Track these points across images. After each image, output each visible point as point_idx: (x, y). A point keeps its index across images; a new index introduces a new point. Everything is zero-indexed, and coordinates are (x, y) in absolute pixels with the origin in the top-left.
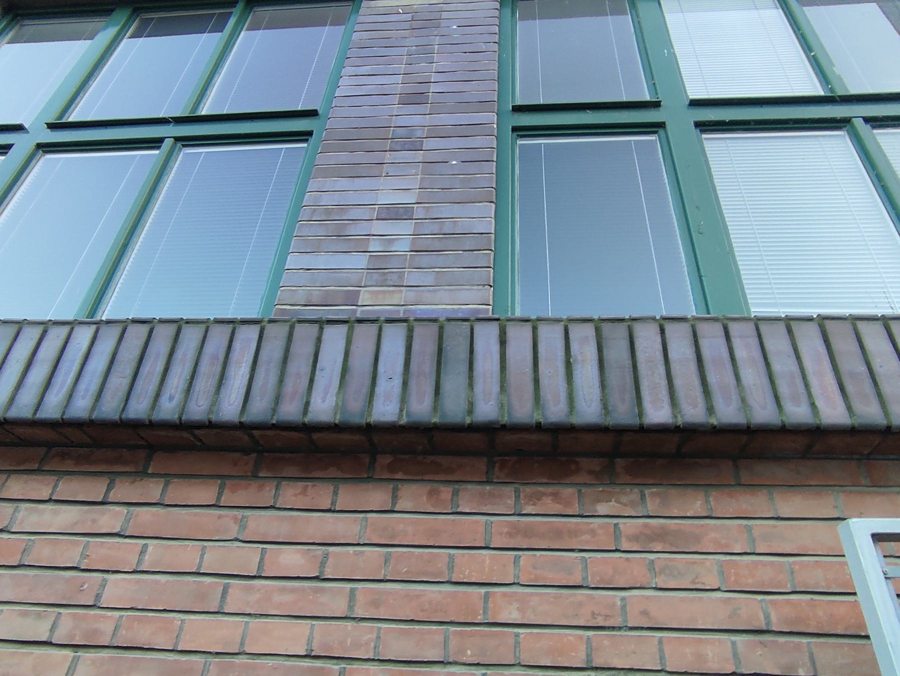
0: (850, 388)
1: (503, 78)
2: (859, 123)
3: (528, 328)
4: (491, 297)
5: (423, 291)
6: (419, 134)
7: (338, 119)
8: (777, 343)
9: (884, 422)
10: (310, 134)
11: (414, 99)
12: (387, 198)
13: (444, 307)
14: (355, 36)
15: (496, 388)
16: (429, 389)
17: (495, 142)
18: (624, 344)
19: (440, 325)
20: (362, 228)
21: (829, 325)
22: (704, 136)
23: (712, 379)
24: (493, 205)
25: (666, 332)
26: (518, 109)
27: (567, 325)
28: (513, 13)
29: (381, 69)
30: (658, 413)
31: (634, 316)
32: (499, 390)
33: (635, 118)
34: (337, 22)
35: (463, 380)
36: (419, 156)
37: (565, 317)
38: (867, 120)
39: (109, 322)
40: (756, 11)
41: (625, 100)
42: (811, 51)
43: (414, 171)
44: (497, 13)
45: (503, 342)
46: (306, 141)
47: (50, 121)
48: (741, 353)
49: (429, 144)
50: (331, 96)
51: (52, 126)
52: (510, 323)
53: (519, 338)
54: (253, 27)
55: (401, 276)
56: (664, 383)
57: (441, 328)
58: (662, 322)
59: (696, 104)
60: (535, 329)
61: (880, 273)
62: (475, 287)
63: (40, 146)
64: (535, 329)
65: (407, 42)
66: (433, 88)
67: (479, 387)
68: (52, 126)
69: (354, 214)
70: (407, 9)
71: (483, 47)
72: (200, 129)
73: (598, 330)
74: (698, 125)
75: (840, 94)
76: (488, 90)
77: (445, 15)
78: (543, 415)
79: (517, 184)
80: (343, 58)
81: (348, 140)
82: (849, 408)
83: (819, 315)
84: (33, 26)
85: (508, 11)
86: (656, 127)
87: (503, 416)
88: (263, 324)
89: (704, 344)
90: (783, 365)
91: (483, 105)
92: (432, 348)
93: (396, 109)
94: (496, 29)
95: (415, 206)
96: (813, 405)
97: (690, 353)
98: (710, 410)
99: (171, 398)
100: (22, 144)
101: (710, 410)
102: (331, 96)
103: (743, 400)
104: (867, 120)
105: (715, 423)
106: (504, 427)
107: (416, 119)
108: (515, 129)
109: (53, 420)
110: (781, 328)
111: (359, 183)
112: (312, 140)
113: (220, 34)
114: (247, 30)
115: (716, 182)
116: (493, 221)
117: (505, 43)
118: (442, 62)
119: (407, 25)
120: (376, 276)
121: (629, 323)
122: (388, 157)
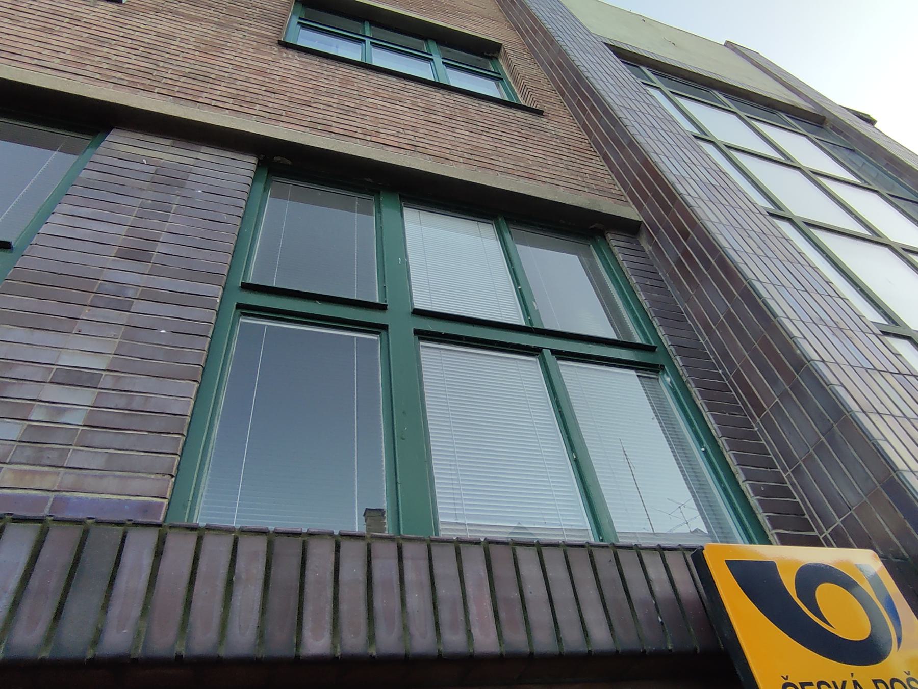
0: (503, 615)
1: (240, 252)
2: (547, 353)
3: (192, 538)
4: (169, 489)
5: (85, 476)
6: (130, 293)
7: (32, 260)
8: (445, 566)
9: (528, 650)
11: (133, 255)
12: (68, 360)
13: (108, 496)
14: (84, 174)
15: (136, 611)
16: (47, 614)
17: (215, 317)
18: (296, 561)
19: (85, 529)
20: (28, 391)
21: (493, 549)
22: (422, 343)
23: (378, 604)
24: (196, 385)
25: (342, 550)
27: (237, 536)
28: (265, 190)
29: (104, 215)
31: (313, 530)
32: (140, 614)
33: (361, 316)
34: (66, 150)
35: (97, 600)
36: (124, 318)
37: (238, 526)
38: (554, 352)
41: (356, 298)
42: (519, 285)
43: (113, 333)
44: (247, 189)
45: (159, 553)
48: (410, 576)
49: (139, 306)
50: (34, 230)
52: (173, 530)
53: (180, 549)
55: (63, 454)
56: (329, 607)
57: (86, 533)
58: (340, 538)
59: (418, 313)
60: (200, 539)
61: (551, 491)
62: (153, 476)
64: (200, 539)
65: (144, 194)
66: (160, 248)
67: (115, 610)
69: (21, 371)
70: (152, 162)
71: (225, 218)
73: (270, 545)
74: (417, 332)
76: (221, 262)
77: (192, 177)
78: (187, 647)
79: (230, 365)
80: (63, 193)
81: (38, 285)
82: (500, 635)
83: (486, 539)
85: (260, 186)
86: (379, 328)
87: (137, 647)
89: (377, 564)
90: (448, 590)
91: (209, 276)
92: (67, 558)
93: (110, 262)
94: (243, 204)
95: (104, 373)
96: (469, 632)
97: (361, 577)
98: (371, 638)
101: (371, 638)
102: (34, 230)
103: (405, 628)
104: (554, 352)
105: (374, 654)
106: (135, 661)
107: (130, 276)
108: (239, 306)
109: (290, 186)
110: (451, 550)
111: (38, 337)
115: (426, 389)
116: (192, 402)
117: (249, 218)
118: (176, 223)
119: (148, 177)
120: (29, 451)
121: (305, 538)
122: (86, 313)
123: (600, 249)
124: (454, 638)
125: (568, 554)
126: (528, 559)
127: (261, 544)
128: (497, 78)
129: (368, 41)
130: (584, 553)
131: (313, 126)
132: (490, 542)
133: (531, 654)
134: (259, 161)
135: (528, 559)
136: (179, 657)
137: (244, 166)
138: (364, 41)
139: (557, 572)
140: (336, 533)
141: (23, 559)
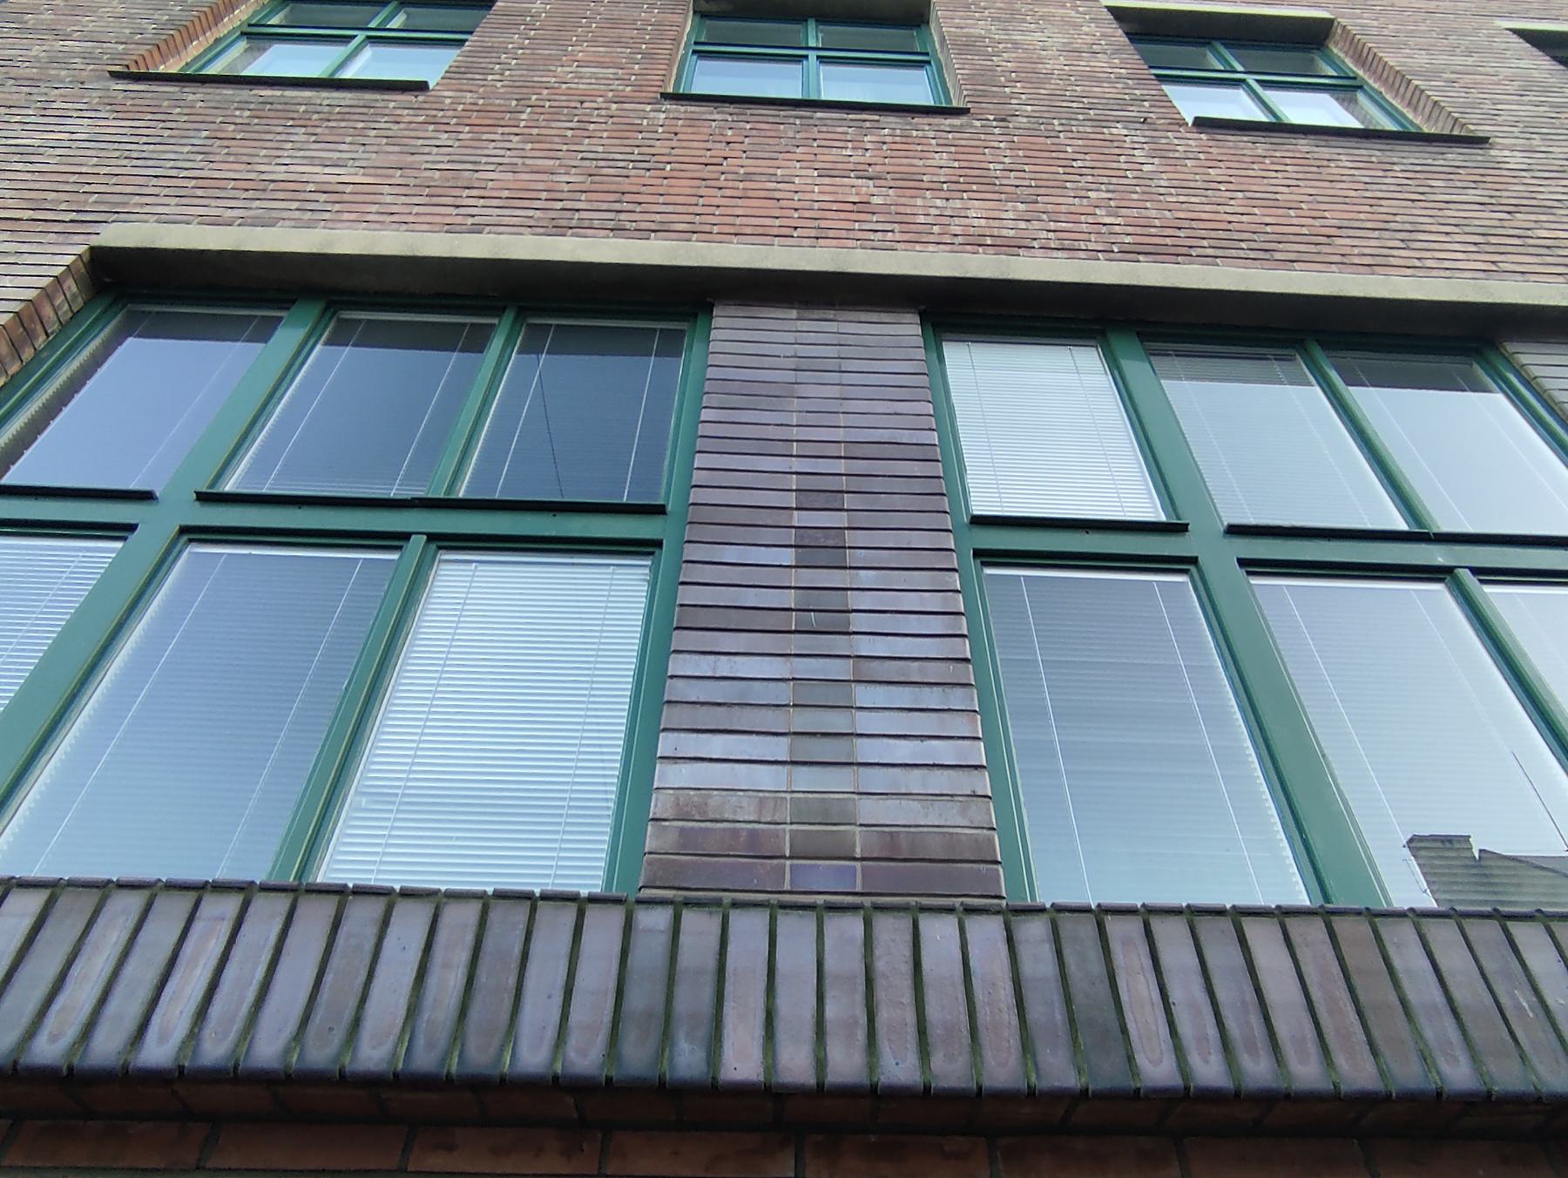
2: (1465, 575)
10: (131, 528)
38: (1475, 571)
46: (124, 539)
47: (199, 489)
51: (203, 498)
54: (335, 341)
59: (1235, 531)
63: (184, 530)
64: (533, 910)
68: (203, 498)
72: (229, 518)
74: (1243, 562)
75: (1435, 530)
83: (1099, 905)
88: (155, 890)
99: (54, 1038)
100: (155, 525)
101: (821, 1063)
104: (1475, 571)
112: (133, 537)
113: (261, 345)
114: (326, 344)
125: (1425, 930)
126: (1172, 936)
129: (812, 55)
130: (1134, 926)
131: (976, 243)
132: (1059, 909)
133: (874, 1088)
134: (920, 314)
135: (1172, 936)
136: (556, 1078)
137: (908, 328)
138: (806, 57)
139: (1222, 955)
141: (27, 923)
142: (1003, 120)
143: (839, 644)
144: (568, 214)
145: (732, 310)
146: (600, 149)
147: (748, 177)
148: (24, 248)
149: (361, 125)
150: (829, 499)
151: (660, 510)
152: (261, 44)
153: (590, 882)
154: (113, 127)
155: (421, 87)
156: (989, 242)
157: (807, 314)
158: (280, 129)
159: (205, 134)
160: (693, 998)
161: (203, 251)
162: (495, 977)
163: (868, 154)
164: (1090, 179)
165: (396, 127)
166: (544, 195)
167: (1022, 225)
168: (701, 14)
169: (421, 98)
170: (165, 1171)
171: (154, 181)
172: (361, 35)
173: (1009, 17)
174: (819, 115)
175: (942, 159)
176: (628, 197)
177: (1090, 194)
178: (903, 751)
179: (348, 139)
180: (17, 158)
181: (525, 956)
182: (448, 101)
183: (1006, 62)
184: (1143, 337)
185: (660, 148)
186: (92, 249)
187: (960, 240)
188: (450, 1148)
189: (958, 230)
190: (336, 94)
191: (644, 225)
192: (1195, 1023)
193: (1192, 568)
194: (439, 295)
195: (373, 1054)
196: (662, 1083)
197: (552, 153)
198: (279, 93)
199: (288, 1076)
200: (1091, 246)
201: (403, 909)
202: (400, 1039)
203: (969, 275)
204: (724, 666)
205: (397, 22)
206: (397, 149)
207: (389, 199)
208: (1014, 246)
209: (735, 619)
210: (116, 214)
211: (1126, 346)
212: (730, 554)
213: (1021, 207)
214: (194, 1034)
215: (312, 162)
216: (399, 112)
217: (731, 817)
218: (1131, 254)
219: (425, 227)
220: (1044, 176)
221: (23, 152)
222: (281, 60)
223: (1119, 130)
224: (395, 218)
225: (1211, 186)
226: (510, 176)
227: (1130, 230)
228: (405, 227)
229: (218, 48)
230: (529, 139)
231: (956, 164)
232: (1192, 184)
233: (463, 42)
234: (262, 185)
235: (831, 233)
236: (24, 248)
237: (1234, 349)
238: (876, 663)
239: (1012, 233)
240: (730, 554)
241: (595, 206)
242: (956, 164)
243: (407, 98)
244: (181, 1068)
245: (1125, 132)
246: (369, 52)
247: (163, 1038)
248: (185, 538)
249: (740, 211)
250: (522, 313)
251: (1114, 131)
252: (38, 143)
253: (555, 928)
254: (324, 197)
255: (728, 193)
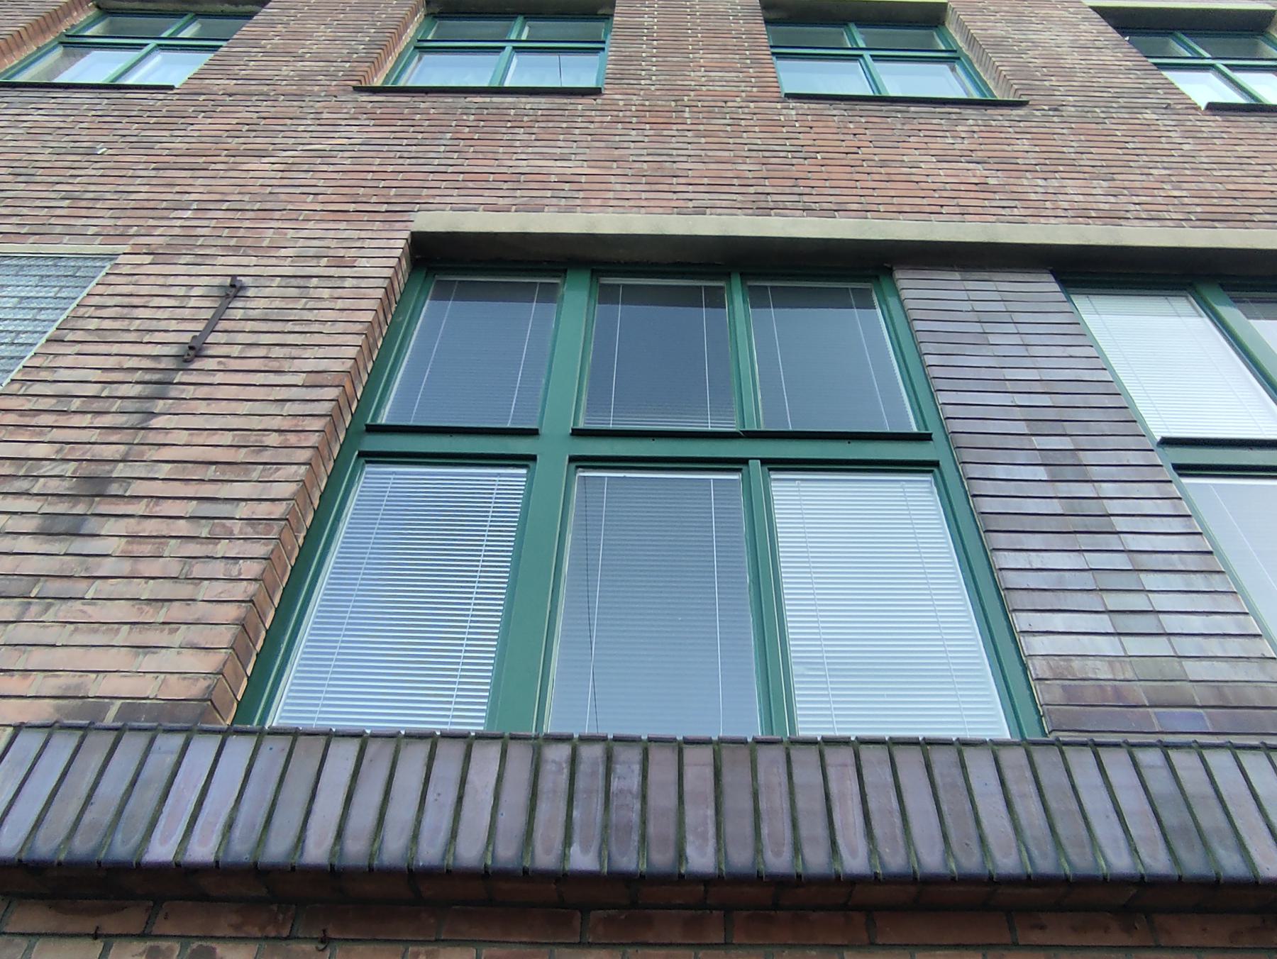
10: (533, 458)
22: (774, 476)
26: (577, 433)
30: (855, 861)
39: (275, 732)
40: (1177, 319)
41: (791, 429)
59: (1167, 442)
83: (754, 739)
84: (1126, 292)
101: (1175, 859)
104: (764, 462)
123: (1206, 302)
124: (1005, 860)
126: (910, 762)
127: (706, 754)
128: (952, 58)
129: (867, 54)
130: (916, 753)
131: (1084, 215)
134: (1052, 272)
137: (1047, 286)
140: (644, 737)
142: (1056, 110)
143: (1113, 542)
144: (763, 197)
145: (910, 274)
146: (759, 142)
147: (883, 164)
148: (363, 234)
149: (564, 125)
150: (1056, 426)
151: (533, 433)
152: (77, 50)
153: (475, 723)
154: (376, 133)
155: (171, 88)
156: (1094, 214)
157: (968, 275)
158: (504, 130)
159: (449, 135)
160: (1210, 818)
161: (496, 234)
162: (1060, 803)
163: (966, 141)
164: (1145, 158)
165: (592, 126)
166: (735, 181)
167: (1112, 199)
168: (433, 16)
169: (599, 101)
170: (1225, 949)
171: (431, 176)
172: (153, 43)
173: (1018, 20)
174: (912, 109)
175: (1024, 145)
176: (801, 182)
177: (1152, 171)
178: (1196, 624)
179: (561, 137)
180: (319, 160)
181: (1074, 787)
182: (621, 103)
183: (1033, 59)
184: (1225, 287)
185: (804, 140)
186: (413, 233)
187: (1070, 213)
188: (1042, 928)
189: (1066, 205)
190: (532, 99)
191: (826, 206)
192: (1143, 827)
193: (936, 470)
194: (676, 264)
195: (317, 852)
196: (991, 877)
197: (724, 146)
198: (488, 100)
199: (953, 879)
200: (1174, 216)
201: (269, 742)
202: (1020, 851)
203: (1091, 243)
204: (1037, 560)
205: (187, 33)
206: (602, 144)
207: (618, 187)
208: (1114, 218)
209: (1028, 523)
210: (425, 205)
211: (1212, 295)
212: (1000, 472)
213: (1104, 184)
214: (262, 840)
215: (544, 157)
216: (588, 113)
217: (1093, 676)
218: (1210, 220)
219: (661, 210)
220: (1110, 157)
221: (323, 155)
222: (97, 67)
223: (1150, 115)
224: (632, 203)
225: (1241, 163)
226: (701, 166)
227: (1197, 201)
228: (643, 210)
229: (402, 65)
230: (699, 134)
231: (1037, 149)
232: (1227, 160)
233: (503, 48)
234: (515, 177)
235: (971, 210)
236: (363, 234)
237: (1264, 294)
238: (1145, 556)
239: (1107, 207)
240: (1000, 472)
241: (780, 190)
242: (1037, 149)
243: (588, 101)
244: (332, 866)
245: (1155, 117)
246: (159, 57)
247: (854, 853)
248: (363, 460)
249: (893, 193)
250: (744, 276)
251: (1146, 116)
252: (328, 148)
253: (450, 757)
254: (567, 186)
255: (877, 177)
